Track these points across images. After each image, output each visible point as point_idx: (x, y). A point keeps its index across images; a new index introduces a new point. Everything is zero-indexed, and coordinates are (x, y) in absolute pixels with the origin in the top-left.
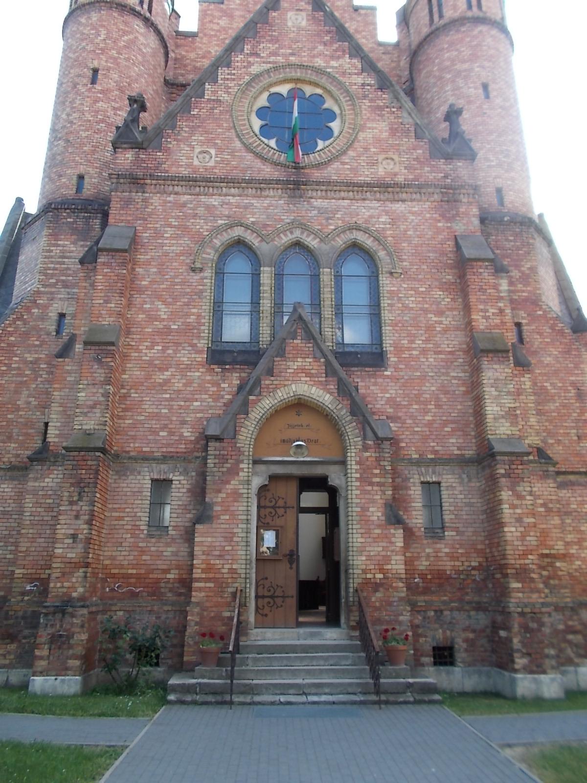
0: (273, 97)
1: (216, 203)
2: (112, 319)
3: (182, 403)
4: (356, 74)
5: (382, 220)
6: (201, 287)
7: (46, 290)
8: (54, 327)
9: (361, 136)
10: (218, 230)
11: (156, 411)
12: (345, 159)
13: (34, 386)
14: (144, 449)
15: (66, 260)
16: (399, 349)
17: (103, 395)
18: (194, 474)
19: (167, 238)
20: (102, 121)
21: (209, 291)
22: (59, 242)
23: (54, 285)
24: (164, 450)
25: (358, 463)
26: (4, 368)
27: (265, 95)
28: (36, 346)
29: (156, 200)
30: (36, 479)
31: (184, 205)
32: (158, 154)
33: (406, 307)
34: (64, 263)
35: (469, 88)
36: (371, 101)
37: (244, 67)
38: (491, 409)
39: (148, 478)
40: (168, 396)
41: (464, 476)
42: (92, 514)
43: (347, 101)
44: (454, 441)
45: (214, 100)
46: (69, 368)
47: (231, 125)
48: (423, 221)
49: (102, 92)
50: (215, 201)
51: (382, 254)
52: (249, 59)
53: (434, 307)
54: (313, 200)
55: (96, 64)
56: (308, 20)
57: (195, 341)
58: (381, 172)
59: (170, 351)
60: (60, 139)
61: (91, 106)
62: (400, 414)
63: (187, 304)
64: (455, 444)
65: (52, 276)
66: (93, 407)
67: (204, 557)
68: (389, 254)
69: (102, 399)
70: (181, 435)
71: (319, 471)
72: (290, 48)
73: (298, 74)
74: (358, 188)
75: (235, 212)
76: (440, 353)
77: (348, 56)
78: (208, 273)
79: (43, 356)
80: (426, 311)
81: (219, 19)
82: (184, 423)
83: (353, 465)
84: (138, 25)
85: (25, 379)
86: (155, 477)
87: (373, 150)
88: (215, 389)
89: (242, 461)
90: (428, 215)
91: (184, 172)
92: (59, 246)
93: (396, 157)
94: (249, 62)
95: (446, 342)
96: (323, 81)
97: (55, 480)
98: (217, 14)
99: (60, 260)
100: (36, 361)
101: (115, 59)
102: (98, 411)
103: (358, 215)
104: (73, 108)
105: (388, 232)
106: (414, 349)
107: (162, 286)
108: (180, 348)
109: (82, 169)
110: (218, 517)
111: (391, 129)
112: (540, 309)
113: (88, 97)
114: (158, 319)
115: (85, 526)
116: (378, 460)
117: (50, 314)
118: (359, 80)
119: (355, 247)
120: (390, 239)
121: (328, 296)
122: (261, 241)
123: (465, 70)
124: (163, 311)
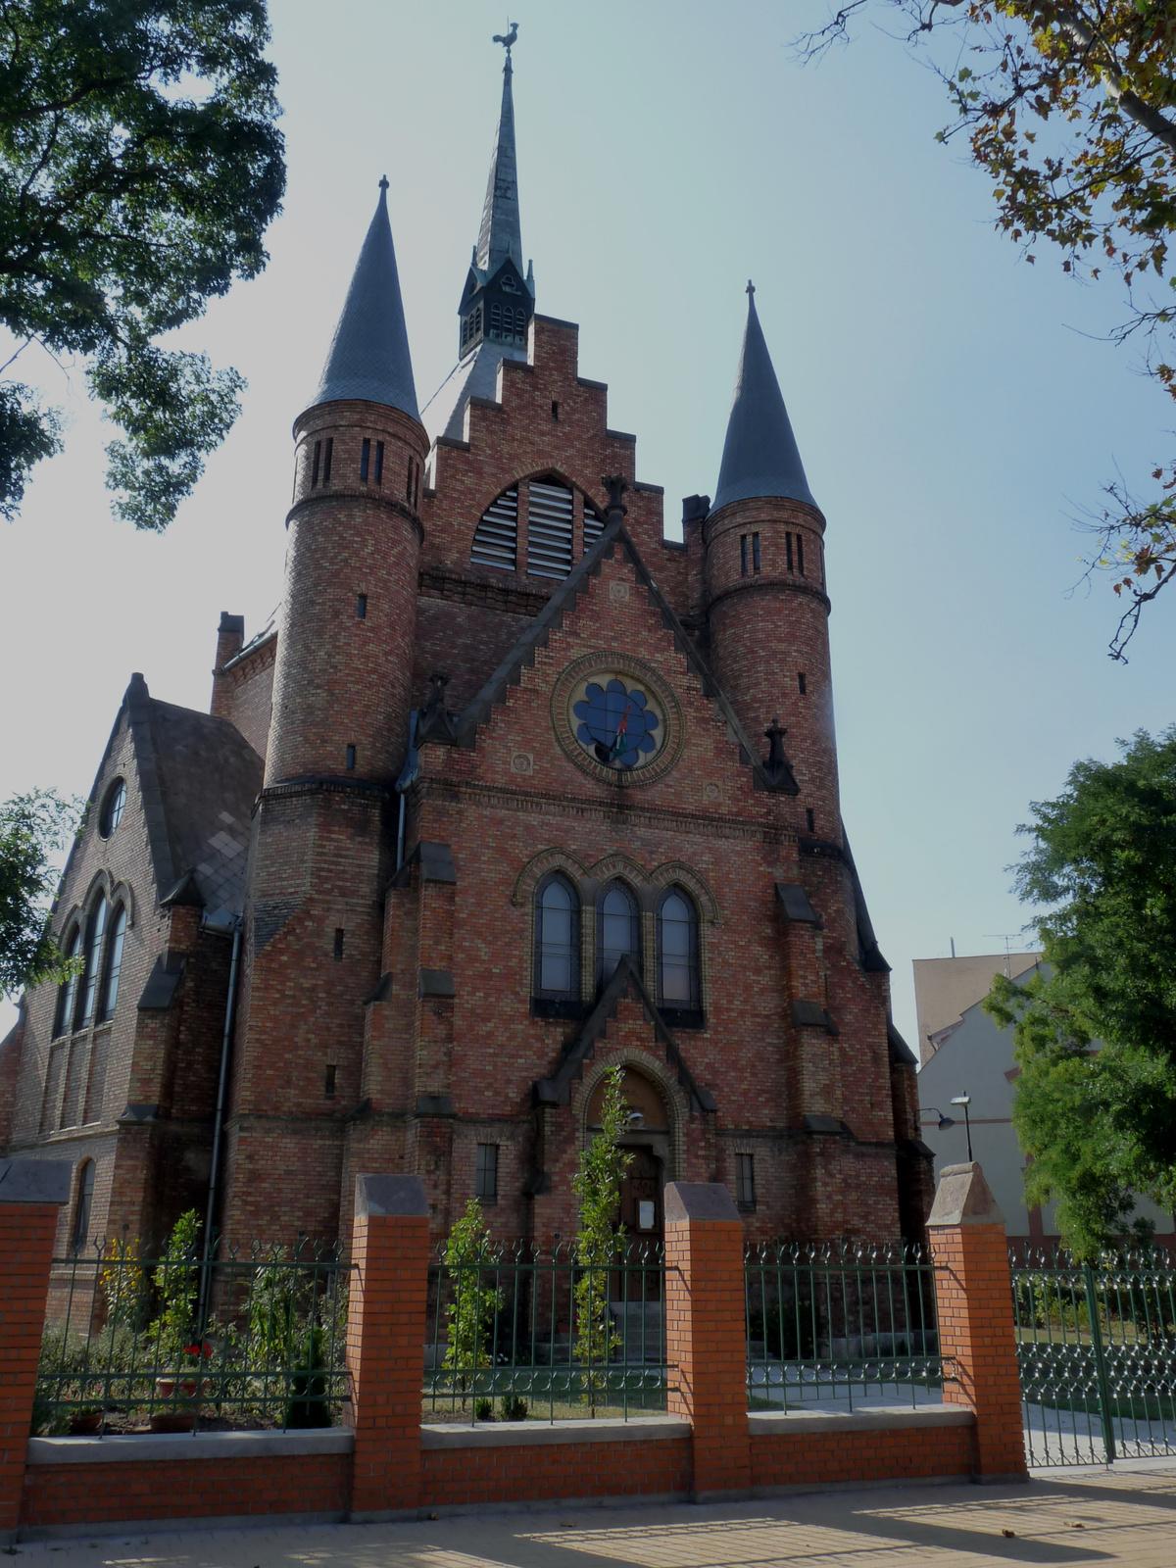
0: (594, 689)
2: (444, 964)
3: (507, 1060)
4: (681, 673)
9: (686, 753)
10: (535, 857)
11: (480, 1067)
12: (669, 780)
13: (313, 1019)
14: (470, 1111)
16: (718, 1010)
17: (445, 1054)
18: (520, 1139)
19: (484, 862)
20: (374, 671)
22: (333, 836)
23: (329, 892)
24: (490, 1111)
25: (685, 1135)
26: (277, 996)
27: (584, 686)
28: (312, 969)
29: (472, 812)
30: (359, 1141)
31: (501, 822)
34: (338, 864)
35: (785, 676)
36: (697, 710)
38: (809, 1085)
39: (475, 1142)
40: (491, 1051)
41: (776, 1149)
42: (449, 1184)
44: (767, 1112)
45: (530, 690)
46: (386, 1013)
47: (551, 725)
49: (372, 629)
50: (534, 819)
51: (704, 899)
54: (636, 829)
55: (363, 588)
56: (631, 595)
57: (518, 989)
58: (705, 800)
59: (493, 999)
60: (318, 687)
62: (718, 1082)
64: (767, 1116)
65: (327, 879)
66: (436, 1067)
67: (544, 1229)
69: (445, 1059)
70: (507, 1096)
71: (645, 1140)
72: (612, 630)
73: (620, 665)
74: (679, 816)
76: (757, 1016)
78: (529, 908)
81: (463, 475)
82: (509, 1081)
83: (681, 1139)
84: (406, 530)
85: (302, 1010)
86: (482, 1141)
88: (539, 1045)
89: (578, 1130)
91: (501, 781)
92: (332, 840)
93: (720, 783)
94: (568, 643)
96: (648, 678)
97: (381, 1142)
99: (335, 859)
100: (313, 989)
101: (386, 581)
102: (441, 1072)
104: (335, 647)
106: (732, 1010)
109: (352, 737)
110: (556, 1187)
112: (845, 960)
113: (356, 635)
115: (443, 1197)
116: (704, 1132)
118: (685, 681)
119: (677, 888)
120: (712, 882)
121: (649, 944)
122: (582, 874)
123: (783, 653)
124: (484, 952)
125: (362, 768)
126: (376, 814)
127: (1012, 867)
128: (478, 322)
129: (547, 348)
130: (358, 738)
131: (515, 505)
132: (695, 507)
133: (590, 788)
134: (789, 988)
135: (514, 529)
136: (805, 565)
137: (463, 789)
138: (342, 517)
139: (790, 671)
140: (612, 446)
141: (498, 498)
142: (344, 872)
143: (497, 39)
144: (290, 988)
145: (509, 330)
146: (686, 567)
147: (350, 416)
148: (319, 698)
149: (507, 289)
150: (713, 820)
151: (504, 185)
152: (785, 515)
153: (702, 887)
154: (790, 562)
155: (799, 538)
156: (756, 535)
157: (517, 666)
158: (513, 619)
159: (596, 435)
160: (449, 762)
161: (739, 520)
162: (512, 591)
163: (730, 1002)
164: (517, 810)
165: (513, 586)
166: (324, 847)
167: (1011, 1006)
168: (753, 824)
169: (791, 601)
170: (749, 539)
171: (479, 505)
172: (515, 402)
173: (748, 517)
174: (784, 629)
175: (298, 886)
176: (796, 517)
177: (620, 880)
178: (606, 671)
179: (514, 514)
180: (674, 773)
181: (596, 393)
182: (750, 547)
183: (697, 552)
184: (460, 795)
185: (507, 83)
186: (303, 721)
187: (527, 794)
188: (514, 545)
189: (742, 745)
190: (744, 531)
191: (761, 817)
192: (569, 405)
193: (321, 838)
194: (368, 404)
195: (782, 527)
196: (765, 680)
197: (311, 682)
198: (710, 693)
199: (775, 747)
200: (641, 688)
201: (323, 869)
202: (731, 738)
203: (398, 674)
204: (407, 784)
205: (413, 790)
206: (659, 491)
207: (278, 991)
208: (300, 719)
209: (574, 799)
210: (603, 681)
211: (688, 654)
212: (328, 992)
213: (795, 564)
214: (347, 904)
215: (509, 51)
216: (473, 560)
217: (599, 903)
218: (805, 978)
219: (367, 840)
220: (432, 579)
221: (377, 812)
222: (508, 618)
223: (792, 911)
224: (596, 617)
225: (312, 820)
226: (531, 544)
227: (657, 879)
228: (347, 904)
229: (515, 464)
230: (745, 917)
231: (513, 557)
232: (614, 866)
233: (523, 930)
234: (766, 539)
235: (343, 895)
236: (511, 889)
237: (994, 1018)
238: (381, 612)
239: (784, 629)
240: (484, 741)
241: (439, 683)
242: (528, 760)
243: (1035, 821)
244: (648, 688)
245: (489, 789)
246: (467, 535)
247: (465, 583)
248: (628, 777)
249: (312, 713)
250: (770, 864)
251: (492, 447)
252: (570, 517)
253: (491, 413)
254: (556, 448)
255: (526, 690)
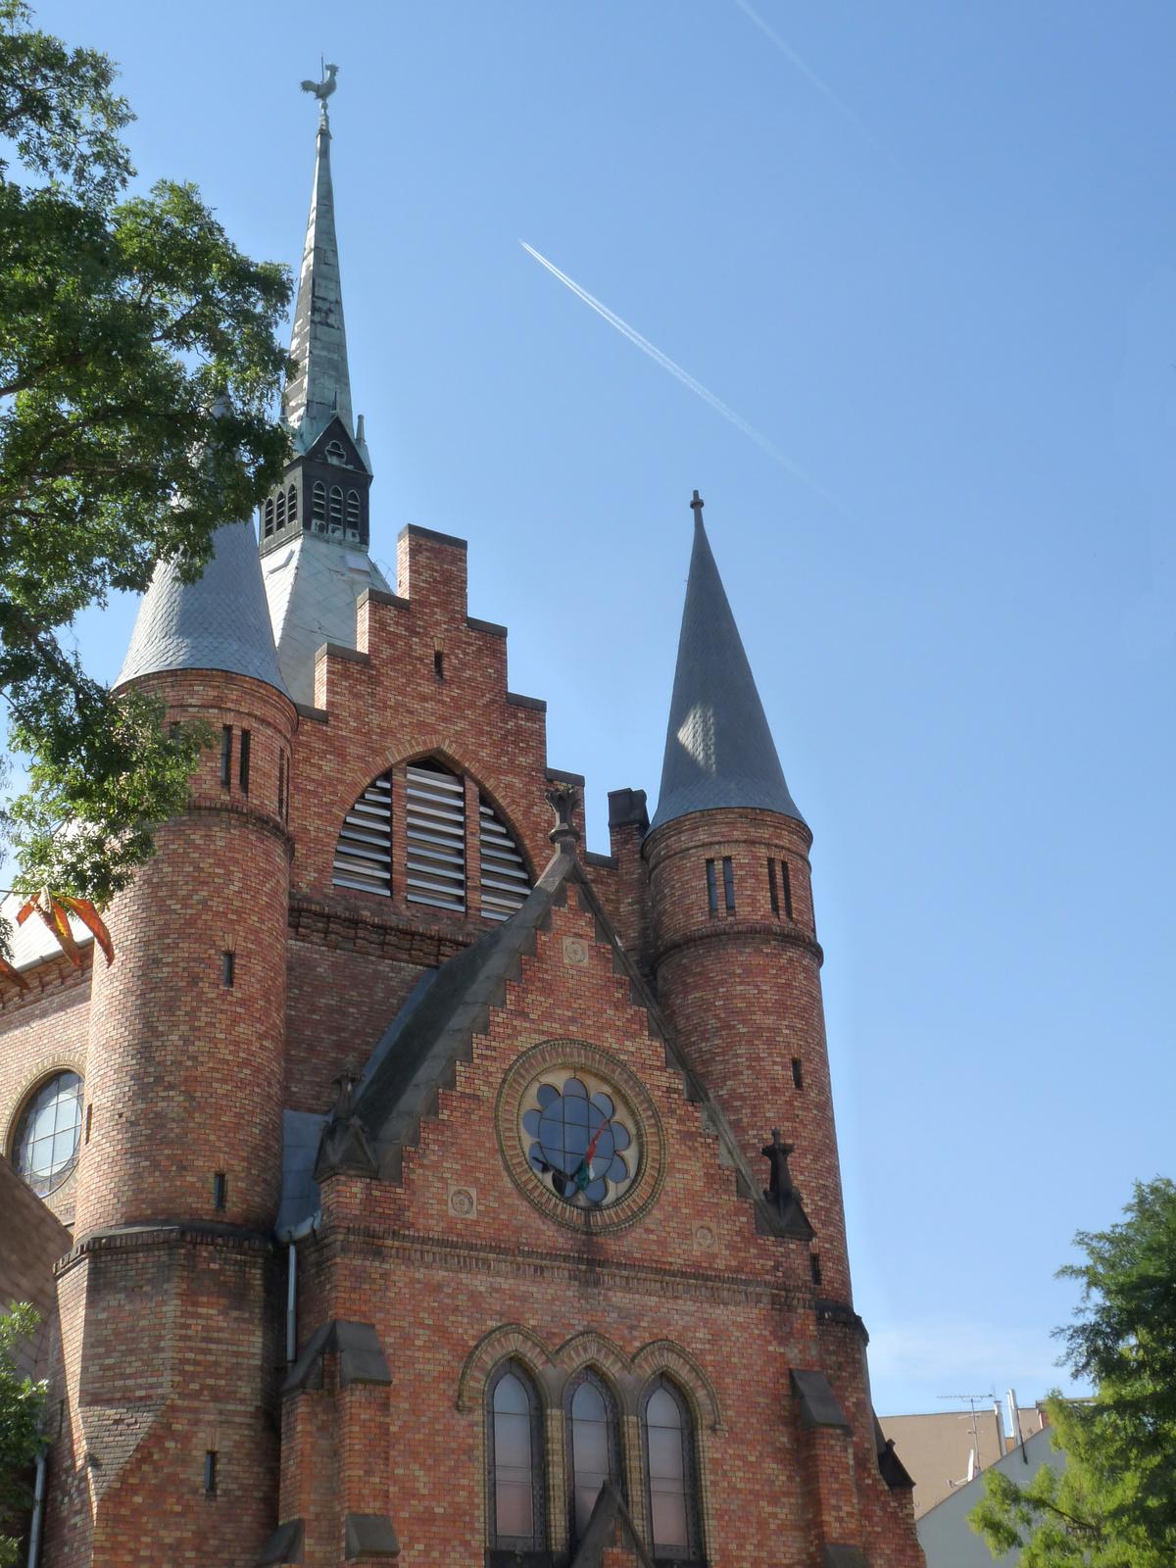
0: (548, 1092)
1: (483, 1289)
4: (659, 1069)
5: (699, 1335)
6: (471, 1441)
7: (186, 1403)
8: (201, 1479)
9: (669, 1183)
10: (486, 1337)
12: (650, 1222)
15: (213, 1346)
19: (420, 1349)
20: (246, 1063)
21: (481, 1448)
22: (201, 1310)
27: (534, 1089)
28: (178, 1514)
29: (400, 1274)
31: (437, 1288)
32: (398, 1190)
33: (734, 1489)
35: (775, 1063)
36: (681, 1121)
37: (509, 1036)
43: (649, 1118)
47: (497, 1147)
48: (750, 1341)
49: (242, 1002)
50: (480, 1282)
51: (701, 1394)
52: (515, 1023)
53: (766, 1488)
54: (610, 1293)
55: (228, 943)
56: (591, 957)
59: (436, 1554)
60: (171, 1087)
61: (228, 1031)
63: (454, 1470)
65: (194, 1376)
68: (711, 1397)
72: (569, 1008)
74: (665, 1276)
75: (509, 1306)
77: (647, 1033)
78: (478, 1416)
79: (188, 1535)
80: (757, 1495)
81: (321, 758)
84: (279, 850)
87: (685, 1211)
90: (756, 1332)
91: (437, 1229)
93: (713, 1225)
95: (782, 1549)
96: (617, 1076)
98: (318, 745)
99: (203, 1345)
100: (178, 1546)
101: (257, 932)
103: (669, 1325)
104: (194, 1029)
105: (709, 1358)
107: (417, 1437)
108: (449, 1548)
109: (222, 1161)
111: (706, 1174)
113: (222, 1011)
114: (414, 1494)
117: (194, 1453)
118: (663, 1079)
119: (666, 1379)
120: (710, 1369)
121: (633, 1464)
124: (422, 1482)
125: (234, 1206)
126: (256, 1276)
127: (1063, 1330)
128: (293, 506)
129: (426, 575)
130: (220, 1162)
131: (387, 800)
132: (626, 805)
133: (550, 1235)
134: (821, 1524)
135: (387, 836)
136: (794, 905)
137: (389, 1242)
138: (197, 838)
139: (783, 1056)
140: (516, 717)
141: (365, 790)
142: (216, 1364)
143: (307, 86)
144: (148, 1546)
145: (336, 521)
146: (617, 891)
147: (202, 693)
148: (172, 1104)
149: (334, 461)
150: (707, 1278)
151: (325, 306)
152: (765, 833)
153: (698, 1377)
154: (774, 900)
155: (784, 864)
156: (727, 860)
157: (451, 1061)
158: (393, 969)
159: (493, 701)
160: (369, 1201)
161: (702, 836)
162: (392, 929)
163: (741, 1547)
164: (460, 1271)
165: (393, 921)
166: (186, 1326)
167: (1010, 1517)
168: (758, 1283)
169: (778, 956)
170: (719, 865)
171: (343, 801)
172: (386, 652)
173: (714, 835)
174: (771, 996)
175: (152, 1386)
176: (779, 837)
177: (592, 1369)
178: (565, 1066)
179: (387, 814)
180: (654, 1212)
181: (493, 637)
182: (720, 876)
183: (632, 871)
184: (385, 1251)
185: (324, 153)
186: (149, 1138)
187: (471, 1247)
188: (387, 859)
189: (738, 1171)
190: (710, 854)
191: (767, 1272)
192: (457, 657)
193: (184, 1314)
194: (228, 676)
195: (762, 851)
196: (749, 1067)
197: (159, 1080)
198: (697, 1093)
199: (778, 1175)
200: (607, 1089)
201: (187, 1361)
202: (725, 1160)
203: (275, 1066)
204: (304, 1230)
205: (316, 1240)
206: (579, 781)
207: (131, 1551)
208: (151, 1131)
209: (530, 1254)
210: (559, 1079)
211: (666, 1040)
212: (198, 1549)
213: (781, 903)
214: (221, 1413)
215: (325, 107)
216: (335, 881)
217: (566, 1404)
218: (838, 1508)
219: (247, 1315)
220: (300, 915)
221: (257, 1272)
222: (385, 966)
223: (817, 1411)
224: (548, 990)
225: (174, 1286)
226: (413, 857)
227: (641, 1367)
228: (221, 1413)
229: (389, 742)
230: (754, 1420)
231: (387, 876)
232: (585, 1349)
233: (472, 1448)
234: (741, 866)
235: (216, 1399)
236: (455, 1387)
237: (989, 1541)
238: (254, 976)
239: (771, 996)
240: (413, 1171)
241: (349, 1087)
242: (470, 1198)
243: (1082, 1259)
244: (617, 1090)
245: (424, 1241)
246: (328, 845)
247: (329, 918)
248: (598, 1218)
249: (163, 1126)
250: (783, 1341)
251: (358, 716)
252: (461, 819)
253: (355, 668)
254: (444, 719)
255: (463, 1095)
